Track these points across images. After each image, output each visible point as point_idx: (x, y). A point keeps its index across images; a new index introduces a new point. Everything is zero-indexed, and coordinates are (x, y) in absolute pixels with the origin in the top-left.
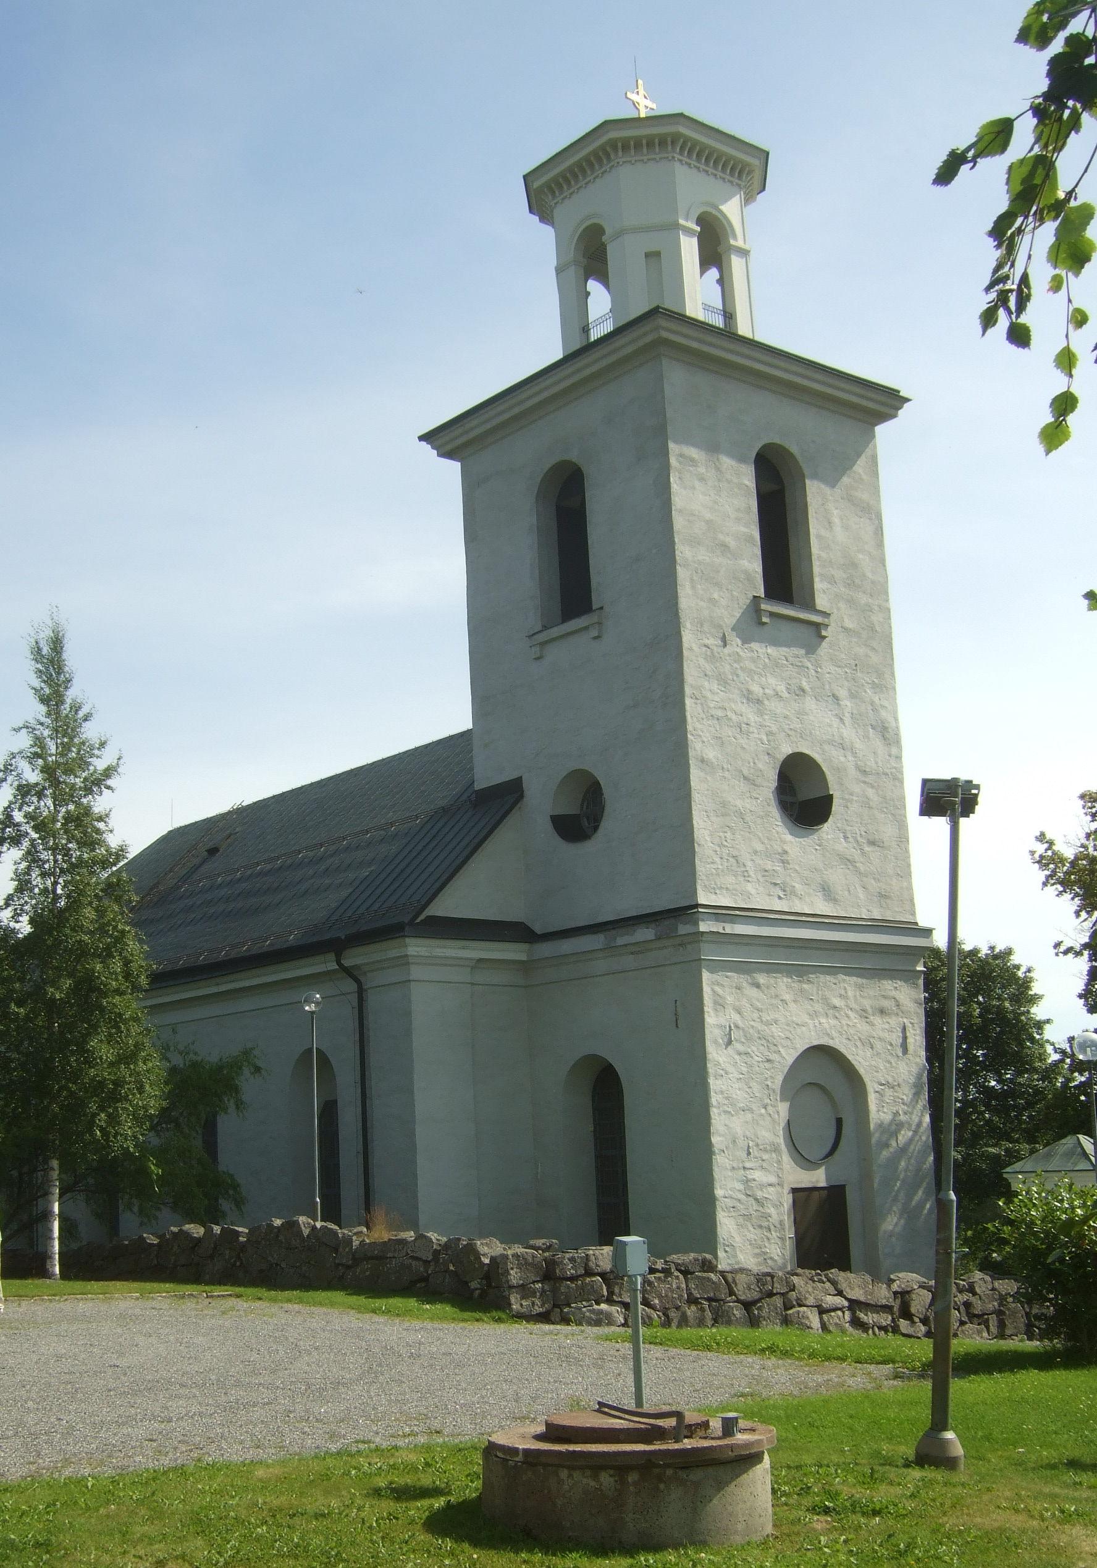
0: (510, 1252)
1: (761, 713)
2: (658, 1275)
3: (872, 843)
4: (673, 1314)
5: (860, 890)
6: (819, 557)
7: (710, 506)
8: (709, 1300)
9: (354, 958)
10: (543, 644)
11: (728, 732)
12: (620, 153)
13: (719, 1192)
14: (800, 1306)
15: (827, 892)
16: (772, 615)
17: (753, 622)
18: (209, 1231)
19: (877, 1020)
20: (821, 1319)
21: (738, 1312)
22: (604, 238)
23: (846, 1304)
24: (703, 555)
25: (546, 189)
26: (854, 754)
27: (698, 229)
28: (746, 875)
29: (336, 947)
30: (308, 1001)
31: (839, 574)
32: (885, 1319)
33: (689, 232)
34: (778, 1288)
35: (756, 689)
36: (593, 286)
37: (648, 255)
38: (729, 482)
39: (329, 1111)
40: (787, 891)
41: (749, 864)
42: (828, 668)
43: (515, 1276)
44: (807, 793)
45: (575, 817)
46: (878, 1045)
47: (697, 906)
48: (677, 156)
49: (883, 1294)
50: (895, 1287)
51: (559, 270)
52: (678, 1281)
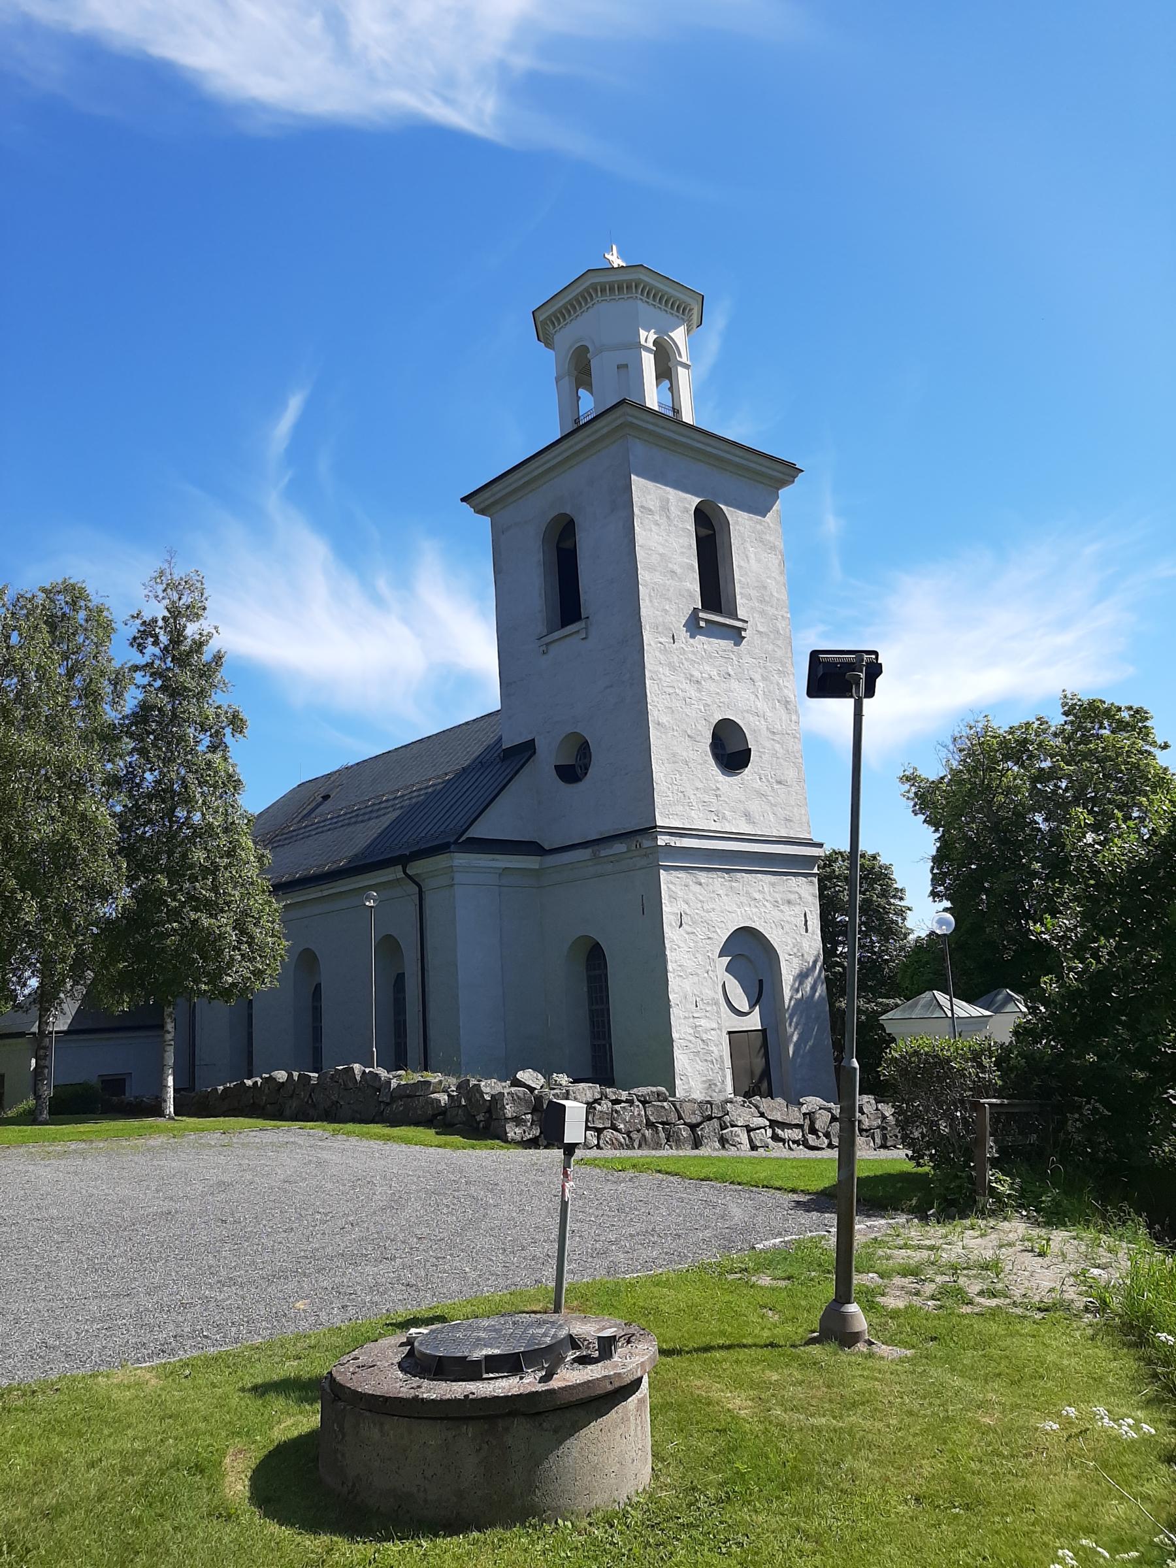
0: (506, 1091)
1: (700, 691)
2: (623, 1105)
3: (779, 783)
4: (634, 1135)
5: (771, 817)
6: (740, 581)
7: (661, 527)
8: (662, 1123)
9: (415, 868)
10: (547, 644)
11: (677, 704)
13: (675, 1035)
14: (733, 1126)
15: (747, 816)
16: (706, 621)
17: (694, 626)
18: (290, 1076)
19: (785, 908)
20: (749, 1136)
21: (685, 1133)
23: (767, 1123)
24: (658, 578)
25: (548, 322)
26: (766, 720)
28: (690, 805)
29: (403, 861)
30: (368, 898)
31: (754, 593)
32: (796, 1134)
33: (648, 350)
34: (717, 1113)
35: (697, 674)
36: (582, 392)
38: (676, 526)
39: (400, 979)
40: (719, 816)
41: (692, 797)
42: (747, 659)
43: (509, 1110)
44: (732, 748)
45: (571, 767)
46: (787, 927)
47: (656, 827)
49: (795, 1116)
50: (804, 1109)
51: (558, 380)
52: (638, 1110)
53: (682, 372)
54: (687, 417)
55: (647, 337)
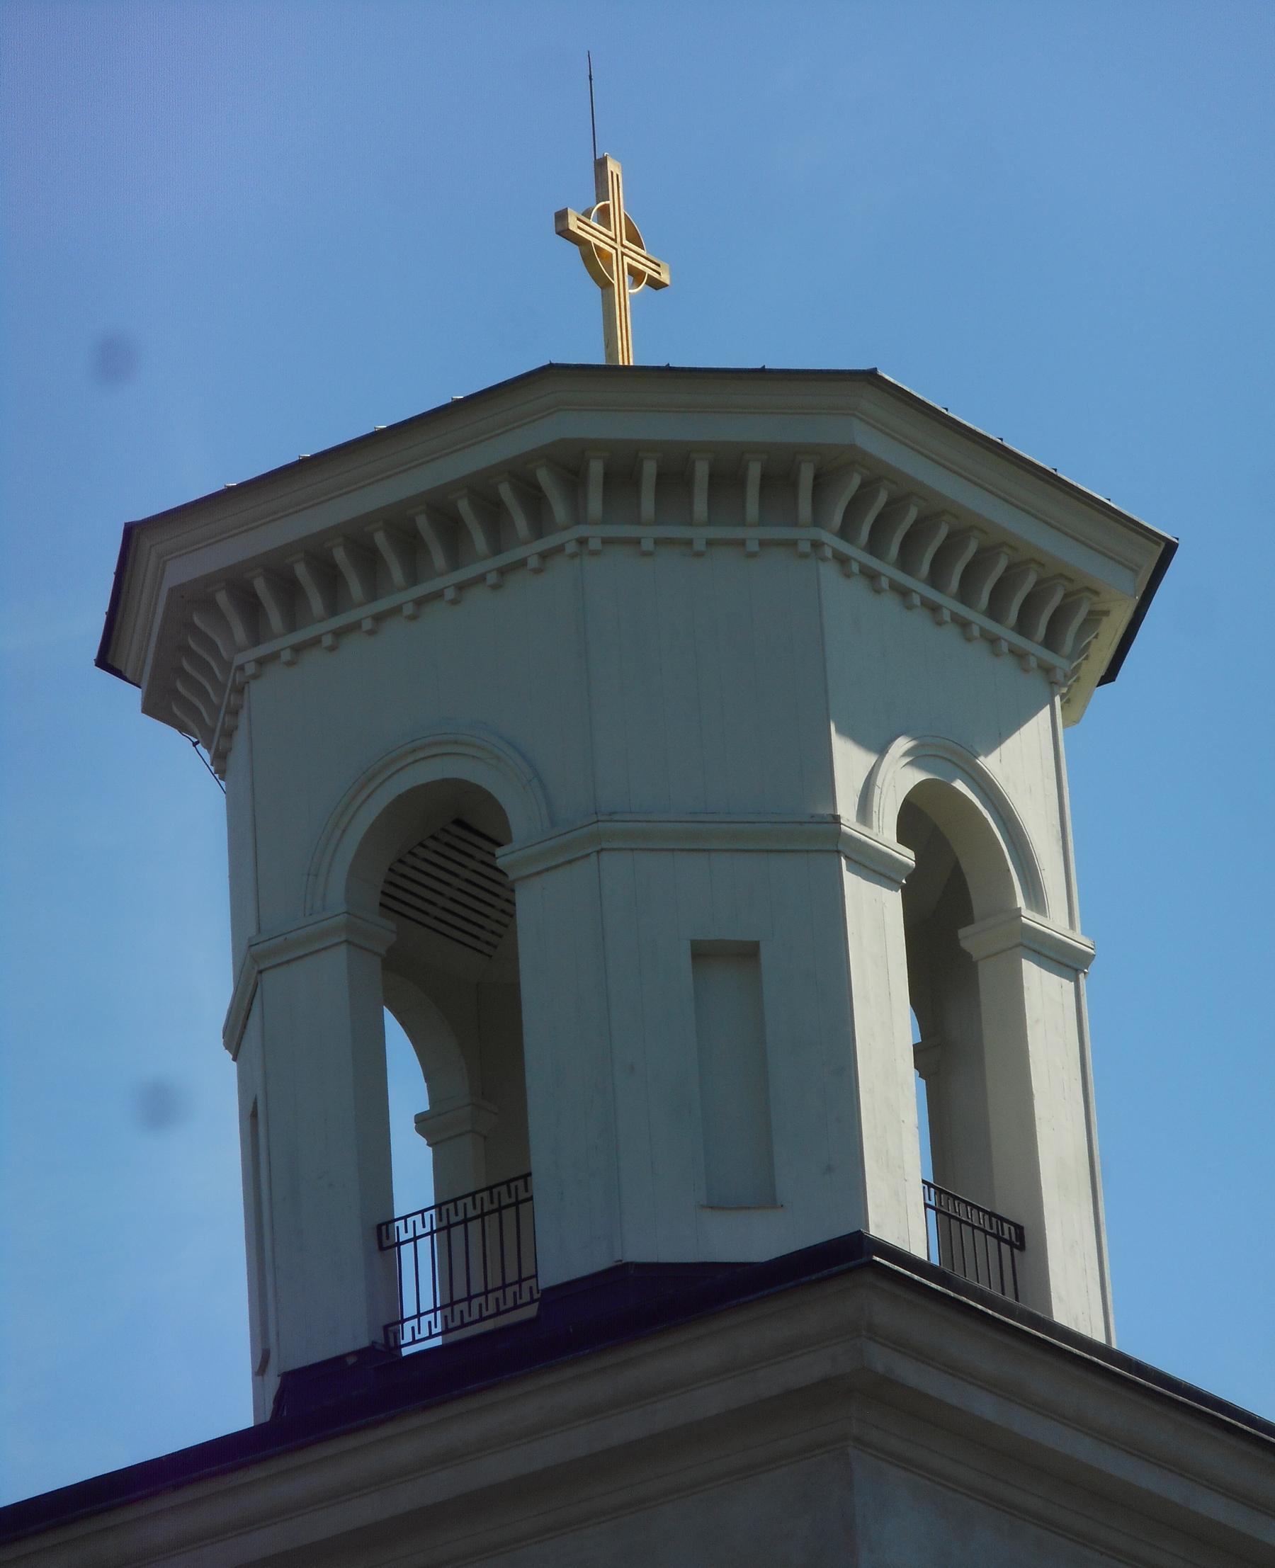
12: (595, 505)
22: (503, 857)
27: (907, 856)
33: (875, 867)
37: (703, 953)
48: (831, 541)
53: (1044, 995)
54: (1076, 1299)
55: (870, 784)
